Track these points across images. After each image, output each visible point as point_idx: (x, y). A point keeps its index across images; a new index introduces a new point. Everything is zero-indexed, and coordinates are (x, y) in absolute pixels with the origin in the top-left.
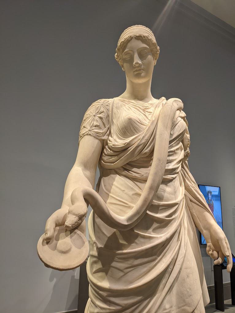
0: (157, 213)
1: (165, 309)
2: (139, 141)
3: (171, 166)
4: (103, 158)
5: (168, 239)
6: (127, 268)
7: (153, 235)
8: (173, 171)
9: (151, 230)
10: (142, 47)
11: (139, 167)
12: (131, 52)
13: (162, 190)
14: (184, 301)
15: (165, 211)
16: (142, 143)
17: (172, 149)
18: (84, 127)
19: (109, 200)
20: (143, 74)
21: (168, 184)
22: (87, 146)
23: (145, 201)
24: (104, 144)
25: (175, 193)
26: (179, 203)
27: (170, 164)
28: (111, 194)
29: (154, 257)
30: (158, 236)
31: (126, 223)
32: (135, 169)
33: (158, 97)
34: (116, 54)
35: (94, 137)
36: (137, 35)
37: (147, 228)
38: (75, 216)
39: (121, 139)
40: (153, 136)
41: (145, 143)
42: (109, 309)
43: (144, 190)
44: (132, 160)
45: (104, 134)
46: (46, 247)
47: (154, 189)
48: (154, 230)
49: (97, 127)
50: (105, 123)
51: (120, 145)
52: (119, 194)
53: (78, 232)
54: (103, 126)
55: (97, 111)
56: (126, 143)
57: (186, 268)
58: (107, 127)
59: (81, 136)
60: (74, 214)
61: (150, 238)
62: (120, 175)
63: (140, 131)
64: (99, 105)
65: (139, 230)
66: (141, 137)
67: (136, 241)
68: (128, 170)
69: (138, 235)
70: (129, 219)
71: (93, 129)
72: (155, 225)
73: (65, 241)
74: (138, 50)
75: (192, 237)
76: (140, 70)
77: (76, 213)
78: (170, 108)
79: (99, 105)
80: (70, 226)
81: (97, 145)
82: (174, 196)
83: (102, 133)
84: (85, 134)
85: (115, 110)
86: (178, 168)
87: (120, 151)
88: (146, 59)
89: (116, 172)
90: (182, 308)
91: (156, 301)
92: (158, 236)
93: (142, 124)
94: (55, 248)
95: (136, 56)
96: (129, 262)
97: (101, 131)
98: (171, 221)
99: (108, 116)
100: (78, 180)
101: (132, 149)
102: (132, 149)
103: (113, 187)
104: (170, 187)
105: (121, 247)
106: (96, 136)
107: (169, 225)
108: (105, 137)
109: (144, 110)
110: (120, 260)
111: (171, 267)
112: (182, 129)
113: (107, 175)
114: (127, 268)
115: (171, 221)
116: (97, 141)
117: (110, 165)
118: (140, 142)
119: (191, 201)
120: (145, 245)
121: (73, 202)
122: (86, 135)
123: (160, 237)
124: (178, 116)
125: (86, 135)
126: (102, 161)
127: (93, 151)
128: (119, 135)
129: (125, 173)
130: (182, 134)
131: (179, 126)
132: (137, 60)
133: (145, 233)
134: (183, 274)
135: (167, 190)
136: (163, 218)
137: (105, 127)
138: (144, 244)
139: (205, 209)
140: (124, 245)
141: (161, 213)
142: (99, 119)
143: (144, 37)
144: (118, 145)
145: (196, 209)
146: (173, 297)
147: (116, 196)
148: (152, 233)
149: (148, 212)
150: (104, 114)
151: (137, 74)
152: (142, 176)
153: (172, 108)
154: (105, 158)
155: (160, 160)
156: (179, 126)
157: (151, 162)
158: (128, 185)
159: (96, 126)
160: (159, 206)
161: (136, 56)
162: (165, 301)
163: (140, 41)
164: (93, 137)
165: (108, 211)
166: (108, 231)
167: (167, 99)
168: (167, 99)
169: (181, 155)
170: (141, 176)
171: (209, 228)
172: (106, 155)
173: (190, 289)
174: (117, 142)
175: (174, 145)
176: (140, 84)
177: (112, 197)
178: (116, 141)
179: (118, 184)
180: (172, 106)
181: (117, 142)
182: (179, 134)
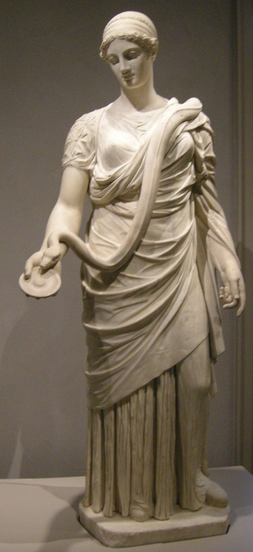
11: (125, 202)
16: (127, 175)
22: (71, 179)
24: (89, 173)
32: (120, 204)
40: (139, 166)
43: (130, 227)
45: (88, 163)
49: (79, 155)
55: (79, 135)
64: (82, 126)
66: (127, 167)
79: (82, 126)
83: (86, 162)
85: (101, 131)
87: (103, 185)
89: (103, 206)
93: (129, 150)
97: (85, 160)
100: (62, 220)
101: (116, 182)
102: (116, 182)
108: (90, 167)
113: (98, 208)
117: (200, 207)
121: (48, 246)
129: (110, 207)
134: (181, 316)
138: (133, 285)
142: (81, 145)
152: (131, 212)
154: (93, 191)
178: (101, 173)
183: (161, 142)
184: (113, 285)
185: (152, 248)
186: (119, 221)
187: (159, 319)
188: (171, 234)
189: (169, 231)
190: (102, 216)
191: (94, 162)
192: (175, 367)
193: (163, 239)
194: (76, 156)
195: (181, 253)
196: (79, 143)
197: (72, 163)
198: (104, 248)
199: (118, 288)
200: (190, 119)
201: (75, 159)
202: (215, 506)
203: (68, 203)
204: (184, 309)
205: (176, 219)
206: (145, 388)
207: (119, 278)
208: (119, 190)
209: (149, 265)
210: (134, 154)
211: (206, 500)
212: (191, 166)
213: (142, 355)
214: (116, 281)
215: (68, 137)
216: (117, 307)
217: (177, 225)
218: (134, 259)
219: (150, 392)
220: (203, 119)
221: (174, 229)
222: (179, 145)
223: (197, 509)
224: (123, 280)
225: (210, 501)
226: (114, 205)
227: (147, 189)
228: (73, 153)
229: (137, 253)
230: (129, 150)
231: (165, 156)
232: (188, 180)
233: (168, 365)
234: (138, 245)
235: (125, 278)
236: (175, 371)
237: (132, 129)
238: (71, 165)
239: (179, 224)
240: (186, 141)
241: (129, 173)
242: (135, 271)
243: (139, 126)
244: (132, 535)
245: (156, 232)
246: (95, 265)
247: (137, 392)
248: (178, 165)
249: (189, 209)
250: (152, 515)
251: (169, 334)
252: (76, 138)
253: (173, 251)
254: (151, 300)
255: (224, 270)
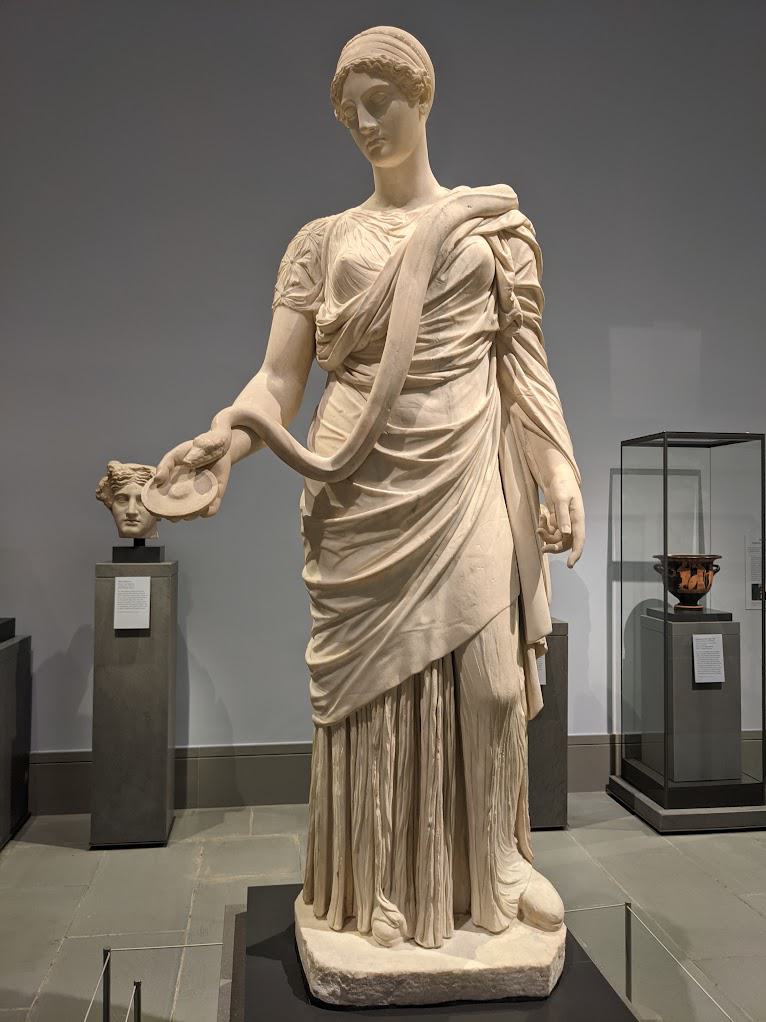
0: (400, 449)
1: (420, 624)
5: (423, 497)
6: (344, 549)
7: (391, 491)
9: (387, 482)
10: (370, 87)
12: (352, 104)
13: (413, 405)
14: (460, 613)
15: (420, 446)
20: (384, 150)
21: (432, 392)
22: (283, 325)
24: (311, 316)
27: (441, 348)
28: (322, 421)
29: (394, 531)
30: (404, 493)
31: (330, 469)
32: (361, 368)
36: (358, 61)
37: (379, 479)
41: (370, 310)
42: (323, 619)
43: (362, 405)
44: (344, 349)
45: (310, 300)
46: (156, 491)
47: (386, 406)
48: (395, 482)
50: (313, 275)
53: (208, 473)
54: (308, 283)
57: (470, 556)
61: (384, 496)
62: (340, 381)
63: (366, 285)
65: (364, 482)
67: (357, 501)
68: (350, 371)
69: (359, 492)
70: (335, 462)
71: (288, 293)
72: (397, 473)
73: (186, 483)
74: (362, 96)
75: (518, 503)
76: (375, 141)
81: (296, 325)
87: (335, 329)
88: (385, 112)
90: (456, 625)
91: (402, 608)
92: (404, 493)
93: (370, 269)
94: (166, 493)
95: (362, 111)
96: (347, 539)
97: (304, 294)
103: (328, 406)
104: (437, 397)
105: (333, 512)
106: (295, 306)
107: (435, 472)
110: (331, 536)
114: (344, 549)
116: (296, 317)
119: (525, 426)
127: (288, 337)
132: (367, 122)
133: (376, 487)
134: (463, 564)
136: (413, 459)
137: (314, 284)
138: (374, 506)
140: (338, 508)
141: (409, 449)
143: (372, 62)
146: (438, 604)
148: (390, 487)
149: (377, 447)
151: (373, 151)
153: (438, 222)
155: (393, 344)
158: (349, 401)
159: (293, 285)
160: (402, 437)
161: (362, 111)
162: (420, 611)
163: (364, 74)
164: (288, 310)
166: (315, 487)
173: (474, 593)
175: (450, 305)
176: (392, 170)
177: (325, 426)
178: (328, 312)
182: (463, 277)
185: (398, 441)
187: (423, 569)
188: (445, 416)
189: (136, 481)
192: (453, 653)
194: (291, 289)
195: (463, 452)
198: (328, 441)
200: (487, 214)
202: (537, 926)
204: (467, 551)
205: (458, 388)
206: (398, 691)
211: (520, 911)
212: (487, 299)
213: (391, 631)
217: (455, 401)
219: (405, 703)
220: (516, 217)
221: (450, 408)
223: (498, 930)
225: (525, 913)
231: (433, 277)
232: (484, 319)
233: (438, 651)
236: (452, 665)
237: (380, 234)
239: (461, 400)
240: (476, 249)
243: (393, 230)
244: (361, 977)
247: (381, 700)
249: (485, 370)
250: (410, 936)
251: (442, 593)
252: (292, 259)
253: (449, 447)
255: (548, 484)
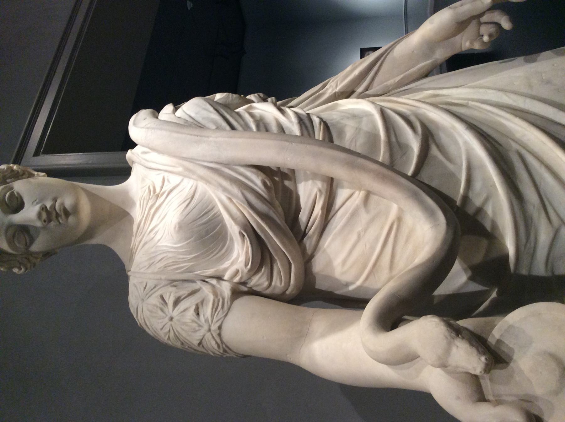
2: (234, 201)
3: (296, 130)
4: (278, 291)
8: (305, 122)
11: (298, 209)
12: (11, 232)
16: (240, 195)
17: (253, 126)
18: (200, 344)
19: (372, 284)
22: (252, 329)
23: (383, 178)
25: (355, 116)
26: (379, 107)
32: (303, 217)
33: (125, 172)
34: (15, 270)
35: (226, 316)
38: (454, 350)
39: (230, 251)
40: (220, 169)
44: (281, 216)
51: (247, 248)
52: (368, 246)
55: (160, 313)
56: (240, 233)
58: (199, 284)
59: (225, 351)
60: (448, 351)
63: (211, 201)
64: (145, 309)
77: (444, 343)
78: (153, 131)
80: (483, 359)
82: (365, 119)
84: (219, 341)
86: (296, 114)
87: (262, 256)
89: (307, 260)
93: (193, 197)
95: (18, 218)
97: (211, 297)
98: (424, 126)
99: (172, 282)
100: (344, 349)
102: (255, 220)
108: (226, 288)
109: (158, 197)
111: (529, 117)
112: (204, 107)
115: (424, 126)
117: (295, 274)
118: (237, 197)
119: (367, 89)
120: (490, 179)
122: (221, 339)
123: (465, 144)
124: (173, 116)
125: (221, 339)
126: (287, 292)
128: (220, 251)
129: (309, 243)
130: (216, 106)
131: (197, 114)
135: (350, 137)
136: (419, 138)
139: (388, 54)
144: (247, 253)
145: (387, 76)
147: (372, 253)
150: (168, 294)
152: (320, 191)
154: (278, 284)
156: (197, 114)
157: (286, 171)
159: (198, 314)
161: (18, 218)
165: (416, 267)
167: (133, 145)
168: (133, 145)
169: (266, 109)
170: (320, 196)
171: (430, 46)
172: (270, 284)
174: (238, 258)
178: (238, 256)
179: (341, 257)
180: (148, 128)
181: (238, 258)
183: (178, 132)
184: (488, 226)
186: (338, 221)
190: (329, 263)
191: (218, 282)
193: (375, 127)
196: (175, 313)
197: (214, 327)
199: (494, 212)
201: (207, 320)
203: (301, 335)
207: (471, 211)
208: (272, 214)
209: (434, 150)
210: (202, 186)
214: (479, 218)
215: (165, 339)
216: (543, 215)
218: (424, 177)
222: (193, 115)
224: (477, 201)
226: (305, 234)
227: (270, 153)
228: (195, 325)
229: (410, 172)
230: (193, 197)
234: (392, 167)
235: (470, 195)
238: (220, 328)
241: (235, 190)
242: (453, 177)
245: (361, 140)
246: (438, 269)
248: (232, 116)
254: (515, 146)
